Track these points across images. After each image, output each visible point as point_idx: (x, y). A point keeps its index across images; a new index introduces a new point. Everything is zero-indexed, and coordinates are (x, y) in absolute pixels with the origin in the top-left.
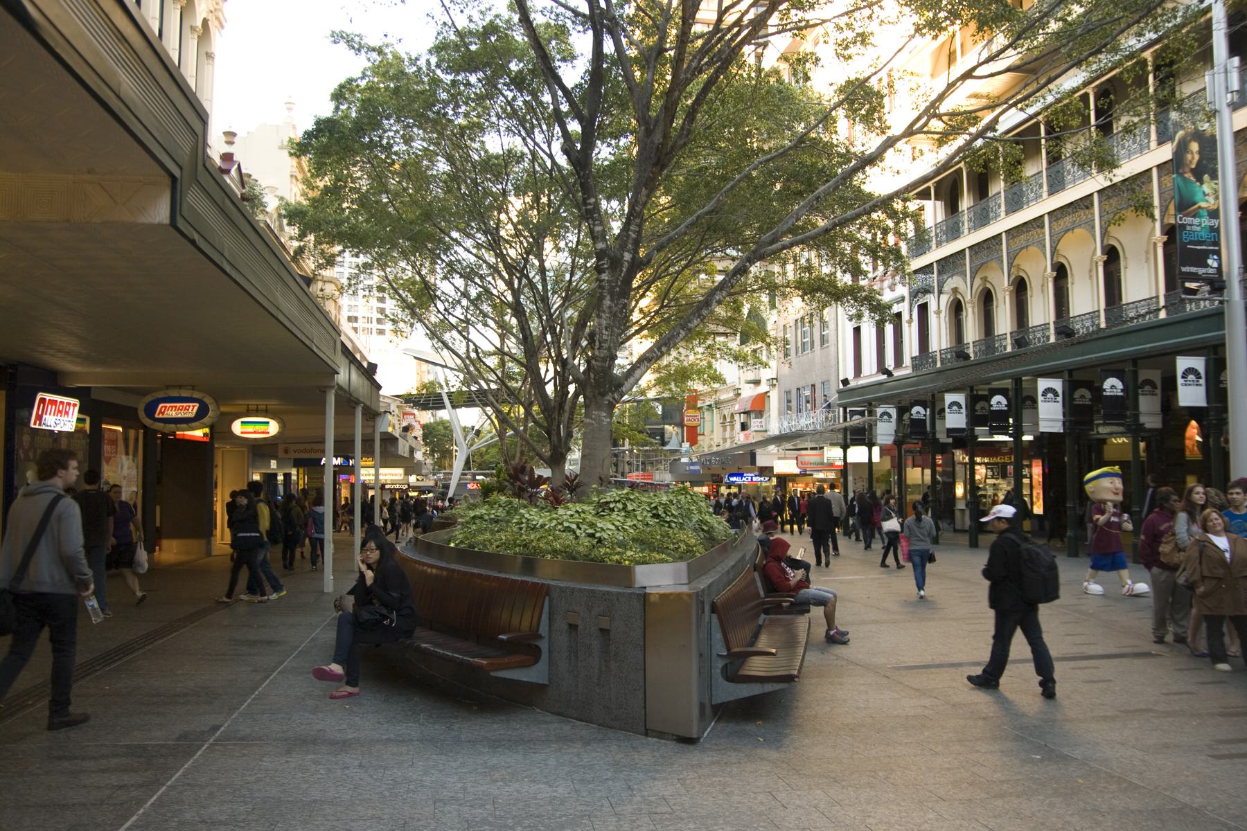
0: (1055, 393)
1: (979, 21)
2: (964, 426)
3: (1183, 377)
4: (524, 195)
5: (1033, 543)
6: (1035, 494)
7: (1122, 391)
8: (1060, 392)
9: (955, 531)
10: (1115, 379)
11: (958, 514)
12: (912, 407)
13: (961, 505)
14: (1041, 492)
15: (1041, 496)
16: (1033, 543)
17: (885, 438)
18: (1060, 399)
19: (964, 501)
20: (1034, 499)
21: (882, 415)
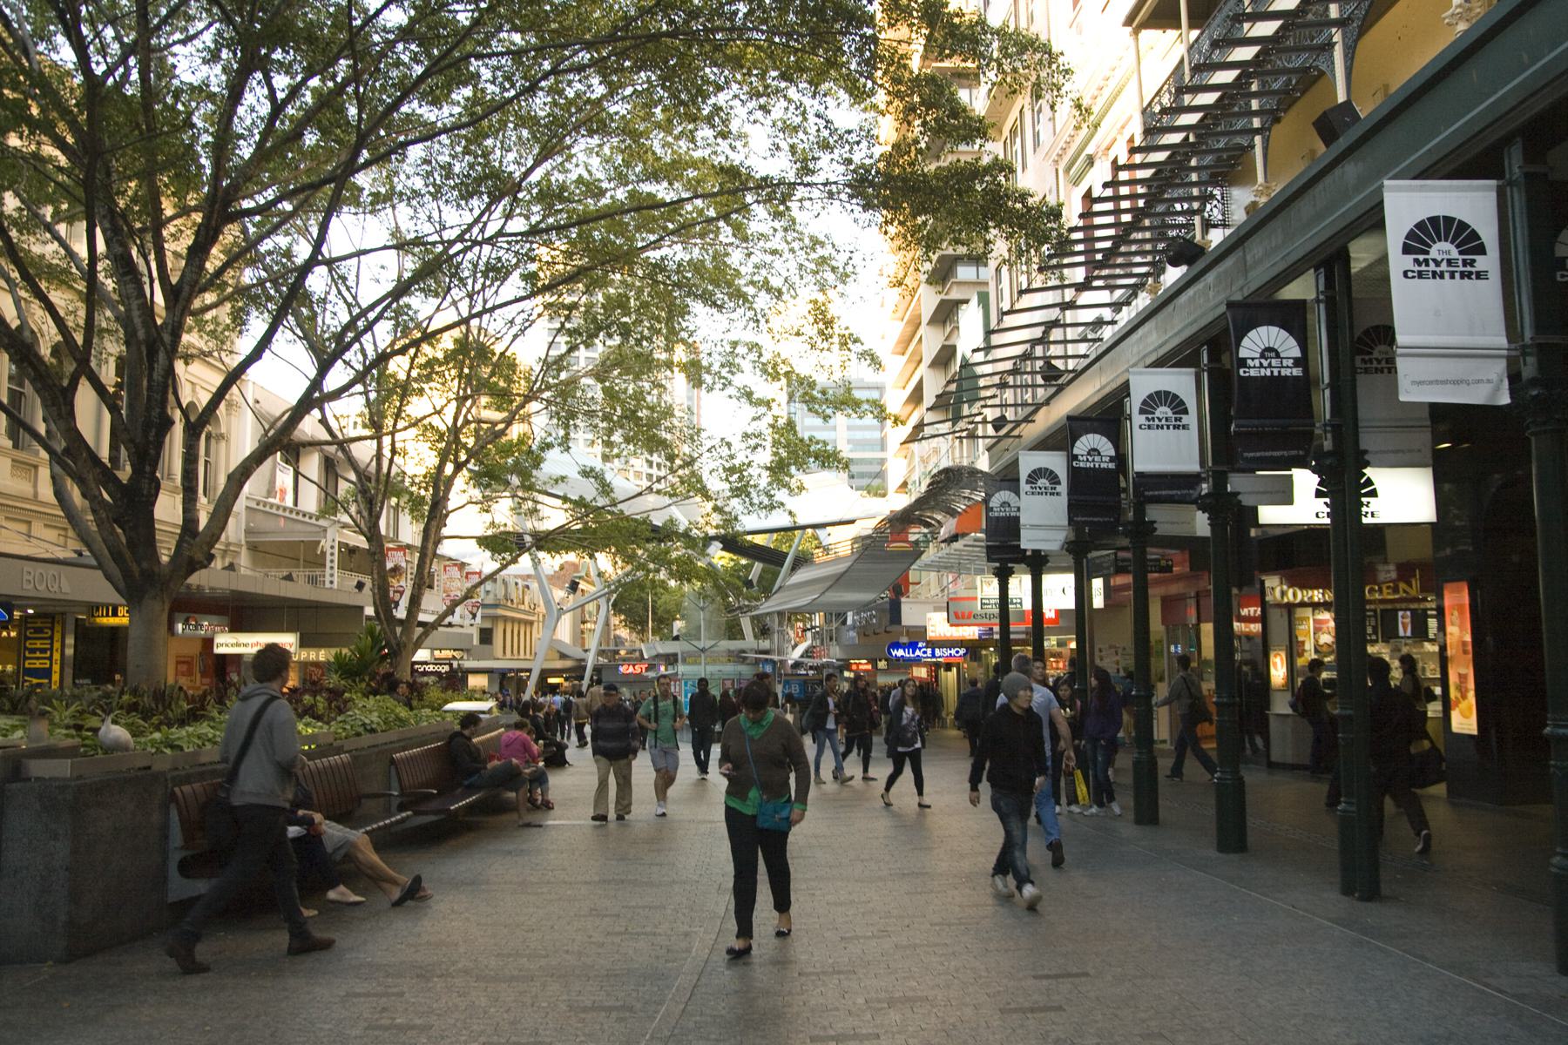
0: (1469, 241)
1: (480, 139)
2: (1195, 467)
3: (1028, 482)
4: (465, 108)
5: (703, 766)
6: (1453, 679)
7: (1112, 459)
8: (1488, 233)
9: (1271, 766)
10: (1274, 330)
11: (1274, 725)
12: (1241, 334)
13: (1281, 706)
14: (1470, 672)
15: (1471, 685)
16: (703, 766)
17: (1041, 534)
18: (1489, 262)
19: (1288, 697)
20: (1453, 693)
21: (1418, 240)
